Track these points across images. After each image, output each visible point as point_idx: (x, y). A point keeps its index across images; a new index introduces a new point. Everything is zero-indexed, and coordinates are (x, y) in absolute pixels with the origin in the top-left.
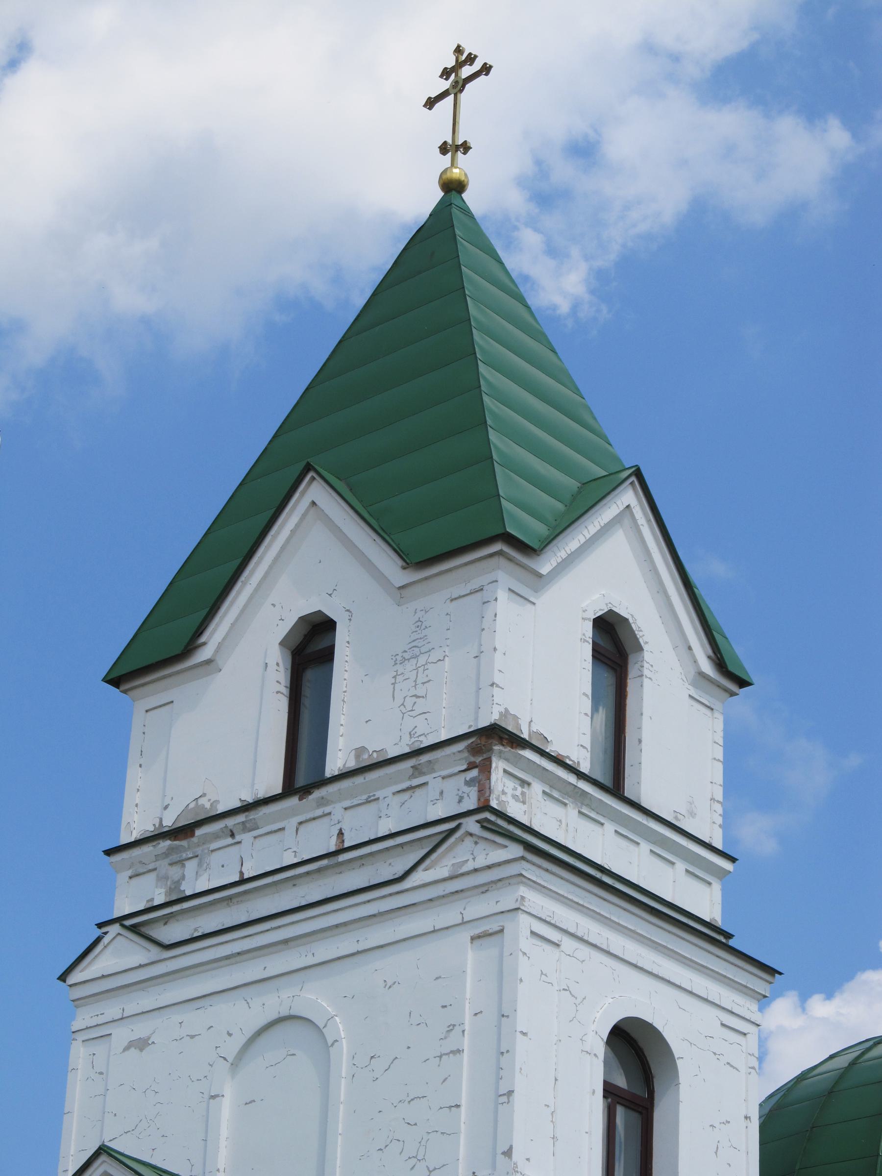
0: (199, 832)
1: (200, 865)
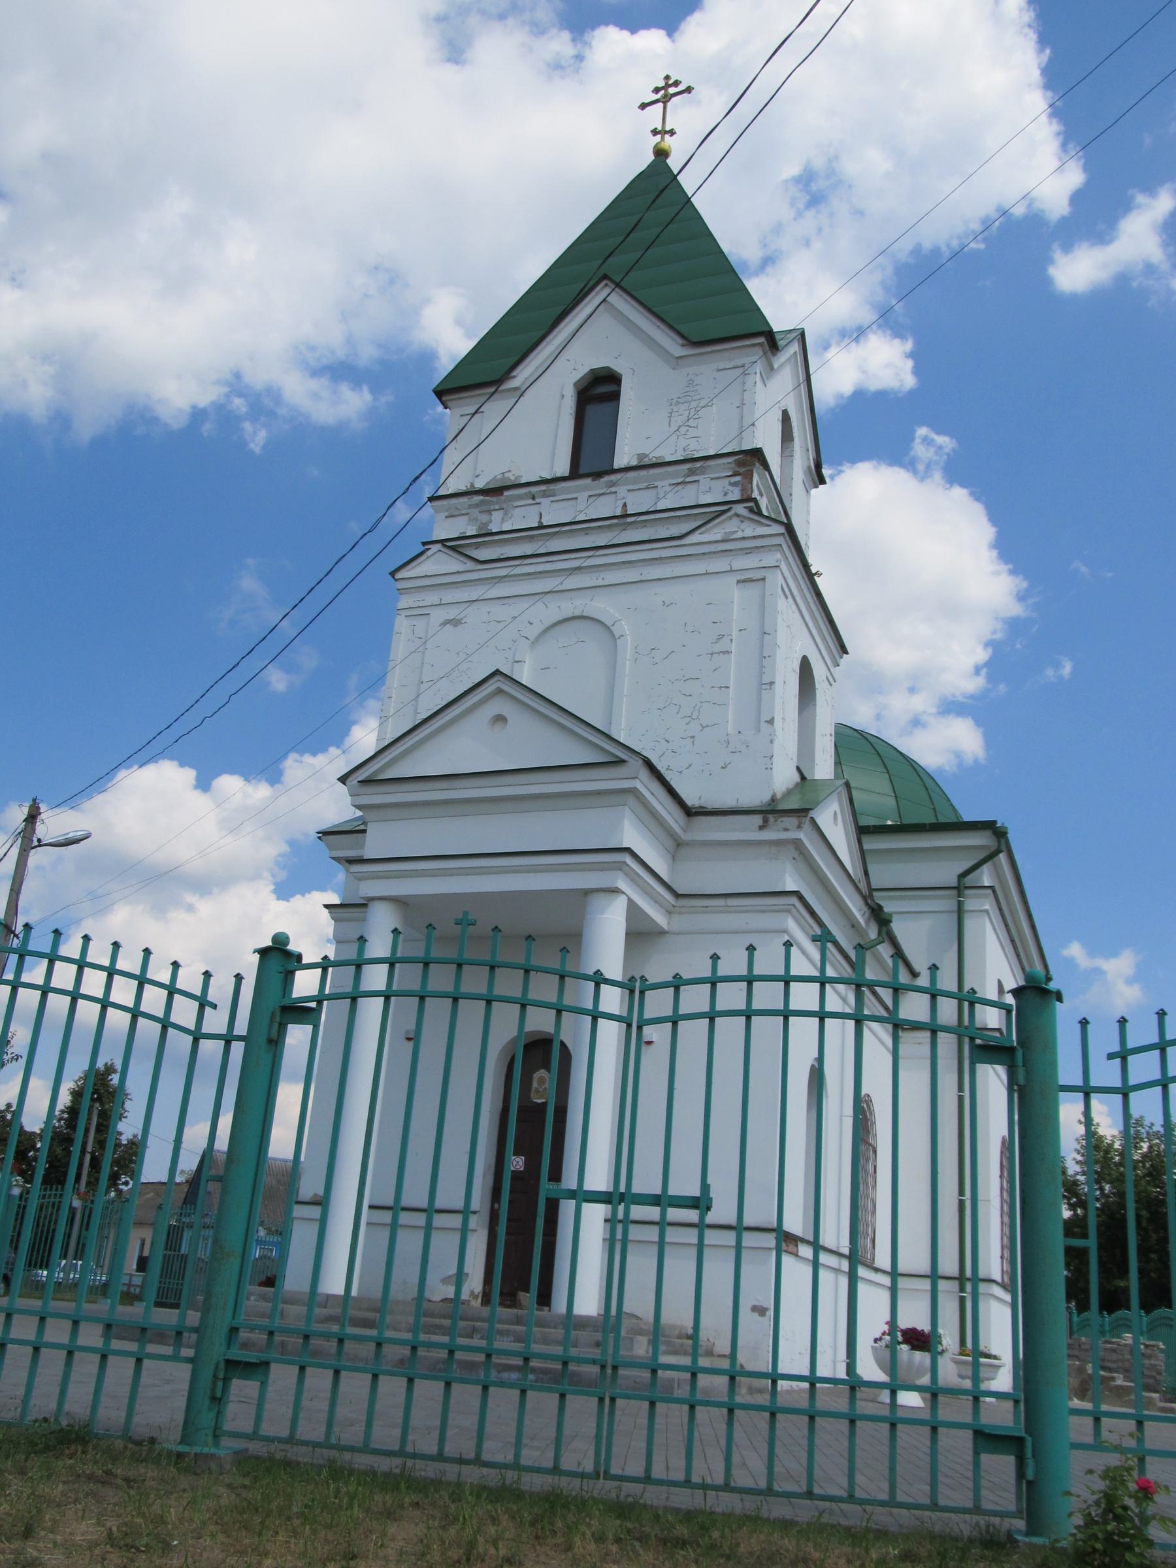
0: (506, 493)
1: (506, 514)
